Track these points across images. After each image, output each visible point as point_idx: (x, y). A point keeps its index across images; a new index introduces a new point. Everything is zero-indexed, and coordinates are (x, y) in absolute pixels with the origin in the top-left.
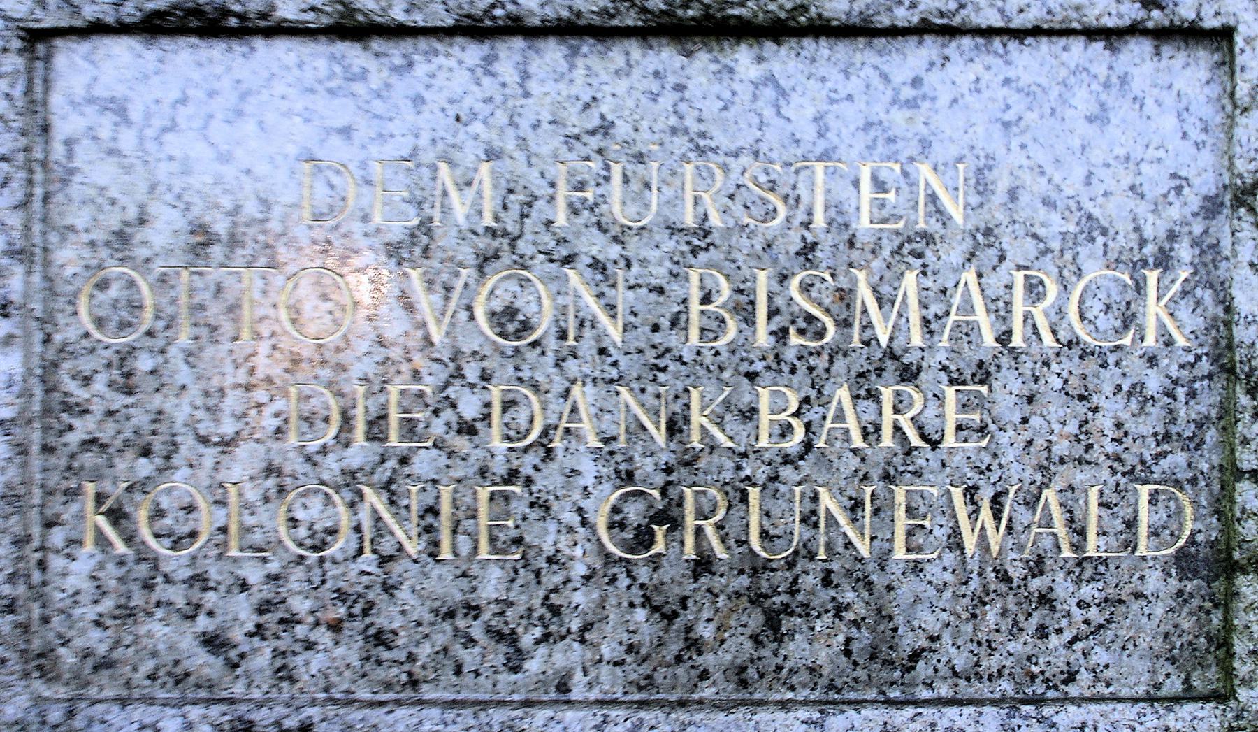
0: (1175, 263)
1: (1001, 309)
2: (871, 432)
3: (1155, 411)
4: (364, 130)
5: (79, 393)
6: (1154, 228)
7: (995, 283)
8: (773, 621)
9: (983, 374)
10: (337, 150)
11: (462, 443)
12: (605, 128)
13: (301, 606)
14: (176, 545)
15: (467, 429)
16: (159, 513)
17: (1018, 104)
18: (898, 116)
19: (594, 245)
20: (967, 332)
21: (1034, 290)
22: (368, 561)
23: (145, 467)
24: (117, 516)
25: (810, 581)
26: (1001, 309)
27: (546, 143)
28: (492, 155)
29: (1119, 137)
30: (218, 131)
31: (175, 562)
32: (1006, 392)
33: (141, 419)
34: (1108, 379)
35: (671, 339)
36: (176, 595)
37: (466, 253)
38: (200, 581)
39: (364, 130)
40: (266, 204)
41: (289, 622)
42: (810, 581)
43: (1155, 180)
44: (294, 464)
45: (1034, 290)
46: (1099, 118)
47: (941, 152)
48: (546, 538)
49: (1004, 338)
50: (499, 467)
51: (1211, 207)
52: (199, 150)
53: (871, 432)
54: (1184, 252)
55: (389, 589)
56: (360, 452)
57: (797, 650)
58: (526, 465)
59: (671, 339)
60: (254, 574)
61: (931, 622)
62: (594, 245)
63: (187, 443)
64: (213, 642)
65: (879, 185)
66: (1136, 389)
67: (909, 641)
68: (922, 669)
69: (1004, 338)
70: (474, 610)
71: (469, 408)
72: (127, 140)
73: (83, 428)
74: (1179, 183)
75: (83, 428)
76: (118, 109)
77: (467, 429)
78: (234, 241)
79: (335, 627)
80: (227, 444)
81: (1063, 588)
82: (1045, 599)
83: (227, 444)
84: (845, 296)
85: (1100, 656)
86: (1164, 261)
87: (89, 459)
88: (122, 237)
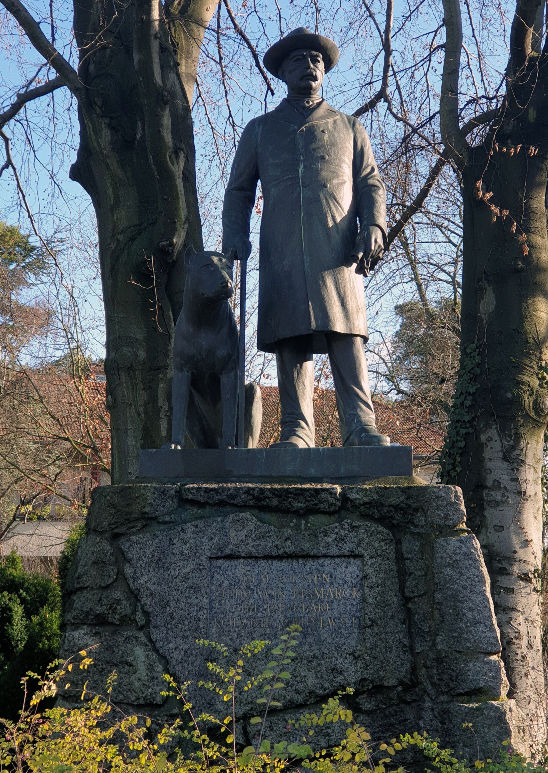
0: (449, 571)
1: (334, 594)
2: (317, 610)
3: (355, 607)
4: (252, 570)
5: (214, 606)
6: (355, 582)
7: (333, 589)
8: (305, 635)
9: (332, 602)
10: (248, 573)
11: (264, 612)
12: (283, 570)
13: (243, 634)
14: (227, 626)
15: (265, 610)
16: (224, 622)
17: (336, 566)
18: (320, 568)
19: (281, 585)
20: (329, 596)
21: (338, 590)
22: (252, 628)
23: (223, 616)
24: (219, 622)
25: (310, 630)
26: (334, 594)
27: (275, 572)
28: (268, 573)
29: (350, 569)
30: (233, 571)
31: (227, 629)
32: (335, 604)
33: (222, 609)
34: (348, 603)
35: (291, 598)
36: (227, 633)
37: (265, 587)
38: (230, 631)
39: (252, 570)
40: (239, 580)
41: (241, 636)
42: (310, 630)
43: (354, 576)
44: (242, 615)
45: (338, 590)
46: (346, 567)
47: (326, 572)
48: (275, 624)
49: (334, 597)
50: (269, 615)
51: (362, 579)
52: (231, 573)
53: (317, 610)
54: (358, 585)
55: (255, 632)
56: (251, 613)
57: (308, 640)
58: (272, 614)
59: (291, 598)
60: (237, 630)
61: (325, 636)
62: (281, 585)
63: (228, 612)
64: (231, 639)
65: (318, 577)
66: (352, 604)
67: (323, 639)
68: (325, 643)
69: (334, 597)
70: (266, 634)
71: (265, 607)
72: (221, 572)
73: (214, 611)
74: (357, 576)
75: (214, 611)
76: (220, 568)
77: (265, 610)
78: (235, 585)
79: (247, 637)
80: (234, 612)
81: (343, 631)
82: (341, 633)
83: (234, 612)
84: (314, 592)
85: (349, 641)
86: (355, 587)
87: (215, 615)
88: (220, 585)
